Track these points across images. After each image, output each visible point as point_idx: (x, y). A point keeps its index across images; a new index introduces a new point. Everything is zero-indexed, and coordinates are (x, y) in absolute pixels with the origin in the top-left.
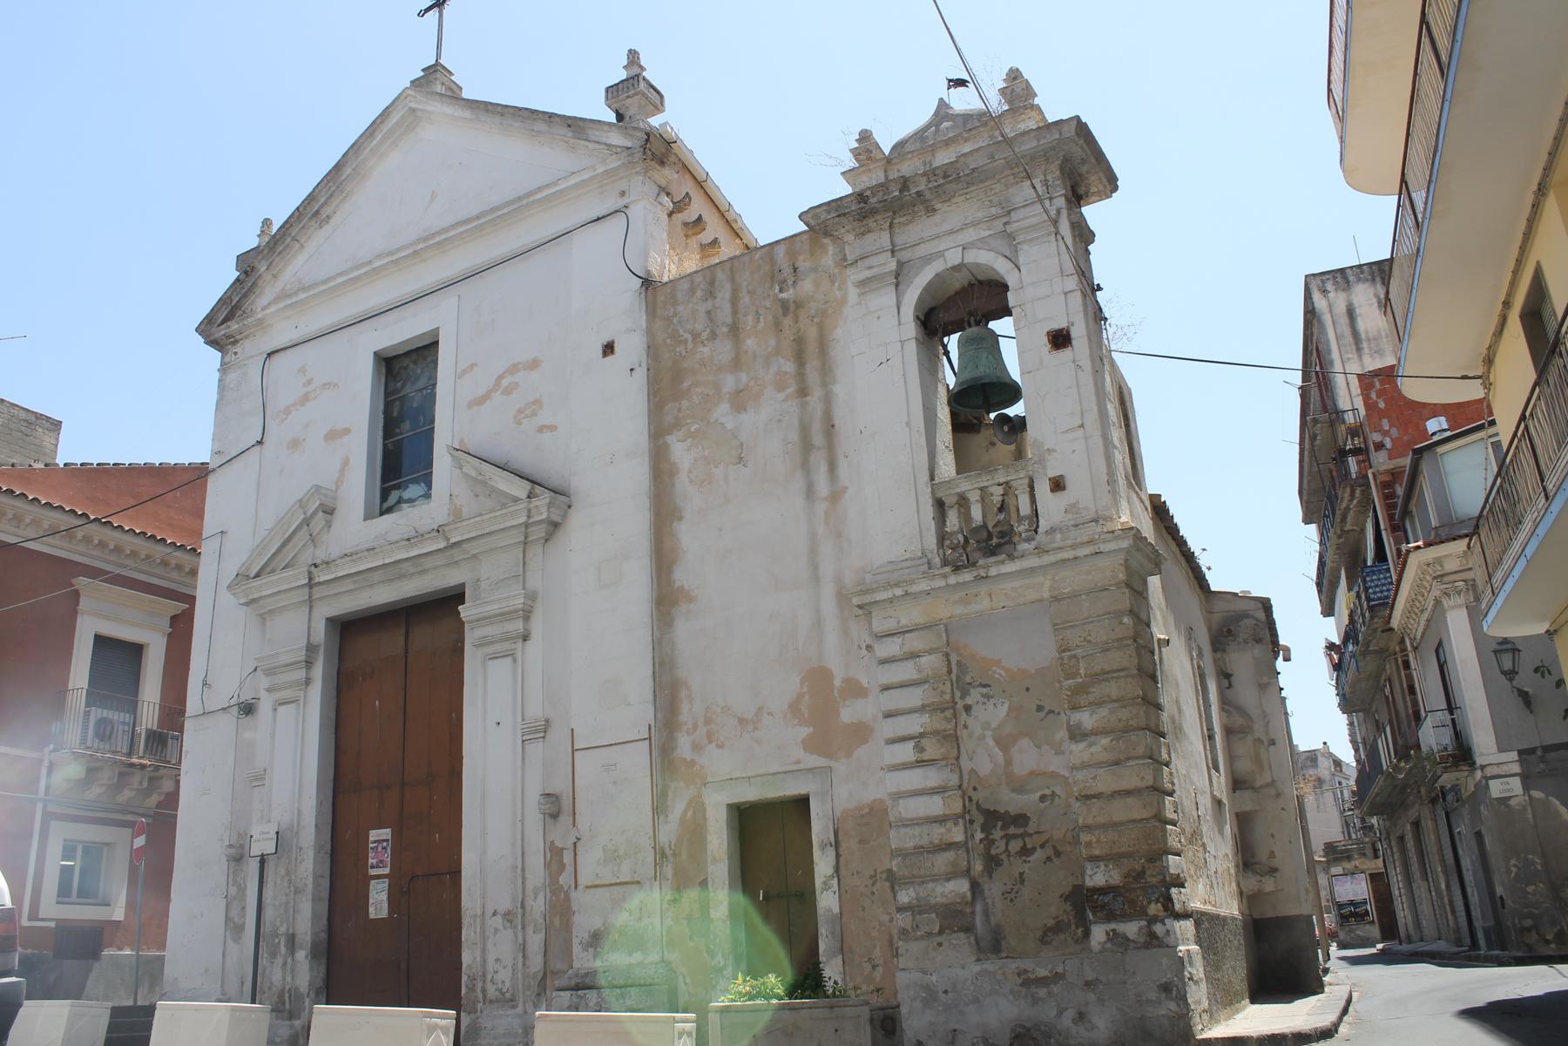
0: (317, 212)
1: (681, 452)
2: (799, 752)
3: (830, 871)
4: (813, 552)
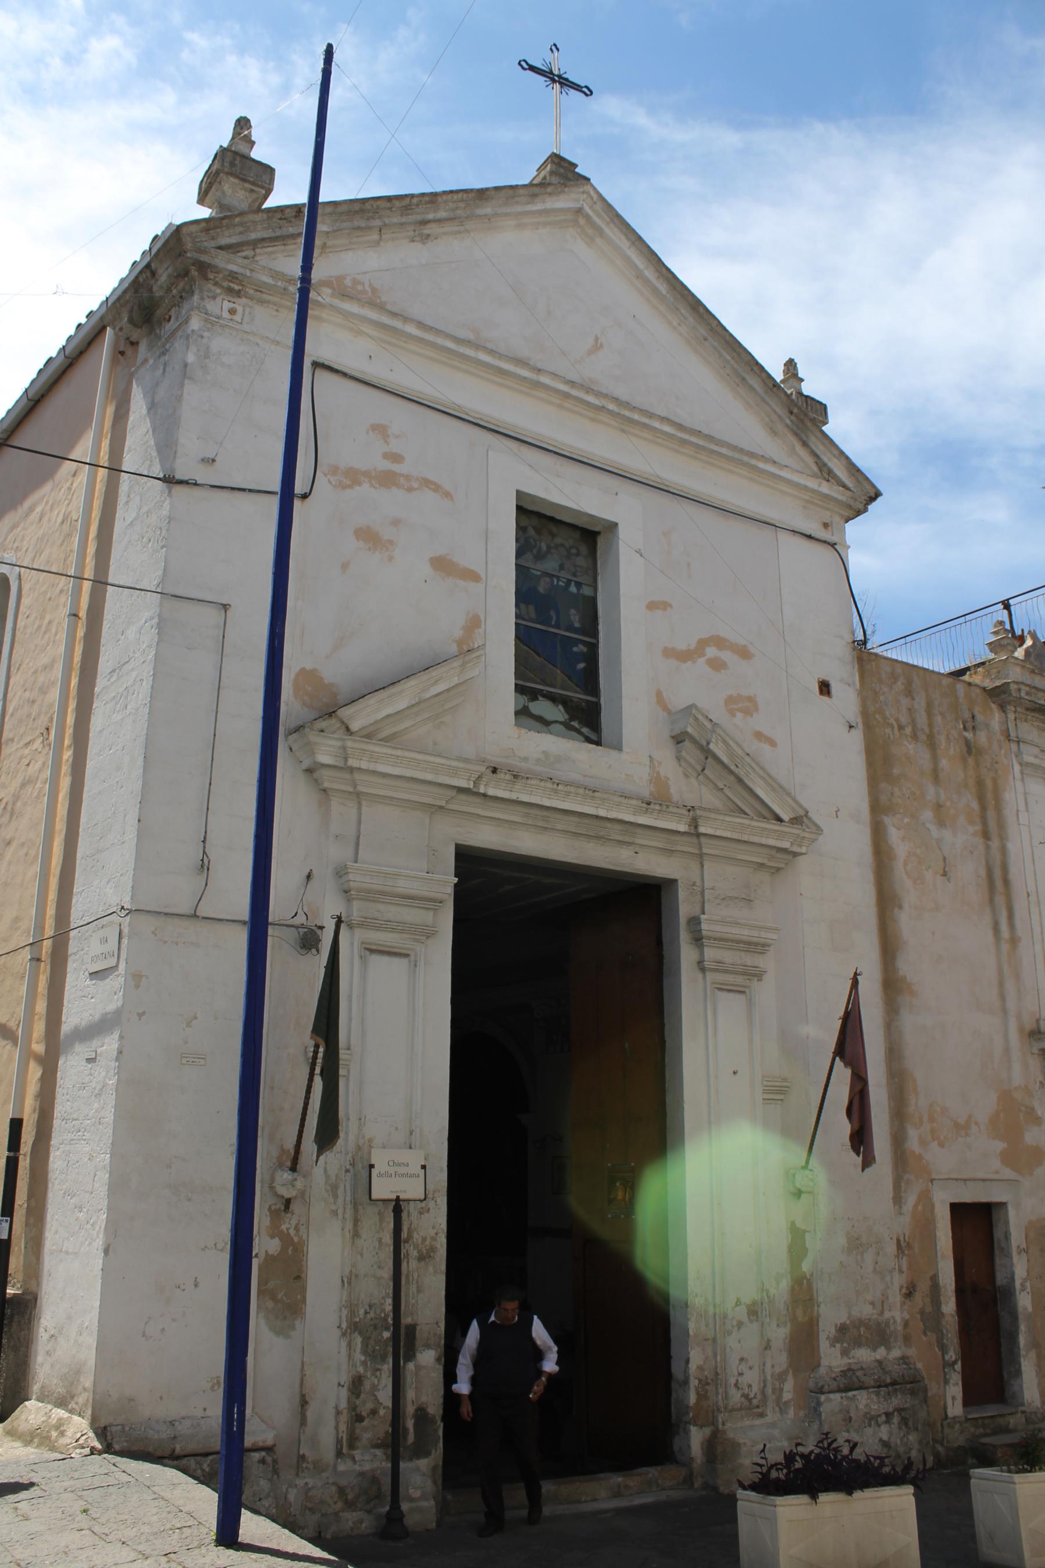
0: (425, 223)
1: (894, 835)
2: (996, 1163)
3: (1024, 1274)
4: (1001, 984)
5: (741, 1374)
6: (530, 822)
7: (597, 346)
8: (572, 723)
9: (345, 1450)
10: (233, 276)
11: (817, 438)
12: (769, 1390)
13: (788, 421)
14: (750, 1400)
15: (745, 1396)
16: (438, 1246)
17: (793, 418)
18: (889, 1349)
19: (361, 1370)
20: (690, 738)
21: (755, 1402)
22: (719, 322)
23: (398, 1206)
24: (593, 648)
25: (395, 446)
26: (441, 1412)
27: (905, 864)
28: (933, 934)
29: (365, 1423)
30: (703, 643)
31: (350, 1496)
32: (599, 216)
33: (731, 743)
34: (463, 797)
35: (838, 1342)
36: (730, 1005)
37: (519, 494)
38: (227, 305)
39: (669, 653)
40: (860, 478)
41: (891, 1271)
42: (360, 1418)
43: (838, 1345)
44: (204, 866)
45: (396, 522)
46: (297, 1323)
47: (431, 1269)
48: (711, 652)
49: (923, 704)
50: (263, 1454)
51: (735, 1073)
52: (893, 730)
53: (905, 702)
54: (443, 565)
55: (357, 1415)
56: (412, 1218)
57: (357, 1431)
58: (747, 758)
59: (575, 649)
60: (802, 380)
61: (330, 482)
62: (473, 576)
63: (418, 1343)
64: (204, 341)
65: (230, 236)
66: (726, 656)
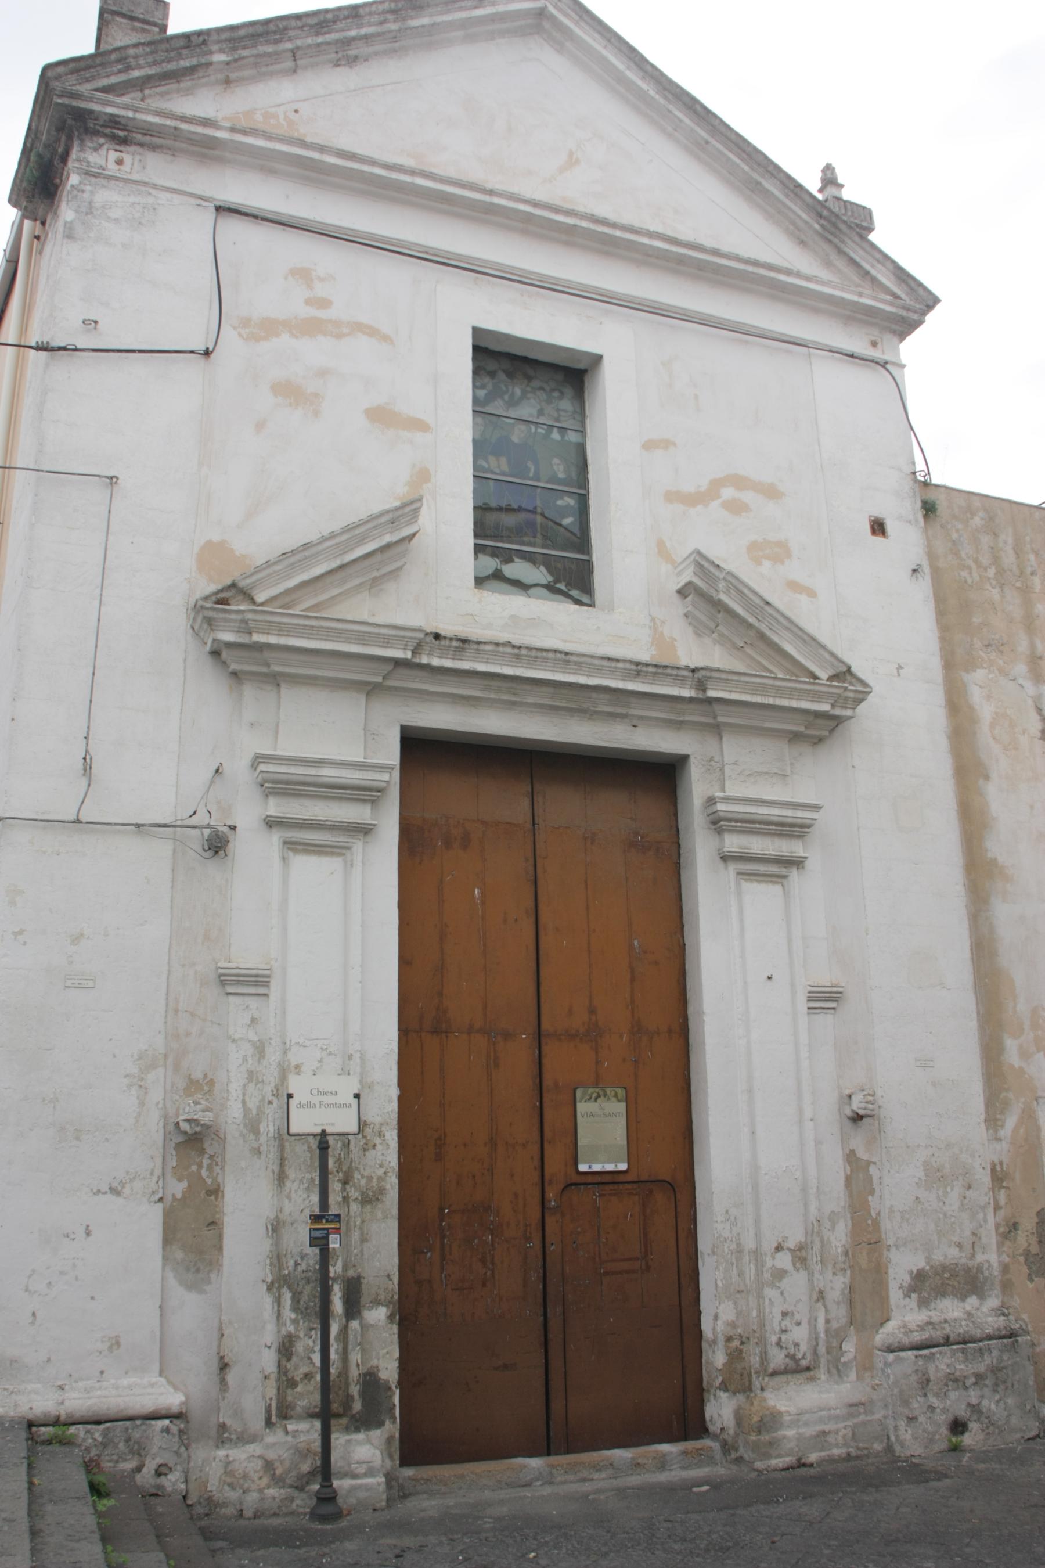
5: (784, 1331)
6: (493, 696)
7: (572, 161)
8: (558, 586)
9: (274, 1419)
10: (114, 122)
11: (855, 242)
12: (822, 1349)
13: (817, 226)
14: (797, 1361)
15: (792, 1357)
16: (388, 1187)
17: (822, 222)
18: (982, 1297)
19: (291, 1329)
20: (708, 596)
21: (804, 1363)
22: (721, 121)
23: (323, 1141)
24: (583, 500)
25: (321, 290)
26: (397, 1376)
27: (992, 726)
28: (1032, 807)
29: (299, 1389)
30: (717, 484)
31: (278, 1472)
32: (566, 15)
33: (746, 591)
34: (402, 671)
35: (914, 1291)
36: (761, 897)
37: (477, 332)
38: (113, 155)
39: (672, 496)
40: (913, 284)
41: (983, 1208)
42: (292, 1383)
43: (914, 1296)
44: (88, 767)
45: (323, 373)
46: (213, 1276)
47: (379, 1215)
48: (728, 493)
49: (1010, 541)
50: (167, 1422)
51: (769, 978)
52: (970, 573)
53: (985, 540)
54: (382, 416)
55: (288, 1380)
56: (352, 1156)
57: (289, 1398)
58: (767, 608)
59: (560, 502)
60: (841, 186)
61: (240, 335)
62: (420, 425)
63: (365, 1299)
64: (86, 195)
65: (108, 76)
66: (748, 497)
